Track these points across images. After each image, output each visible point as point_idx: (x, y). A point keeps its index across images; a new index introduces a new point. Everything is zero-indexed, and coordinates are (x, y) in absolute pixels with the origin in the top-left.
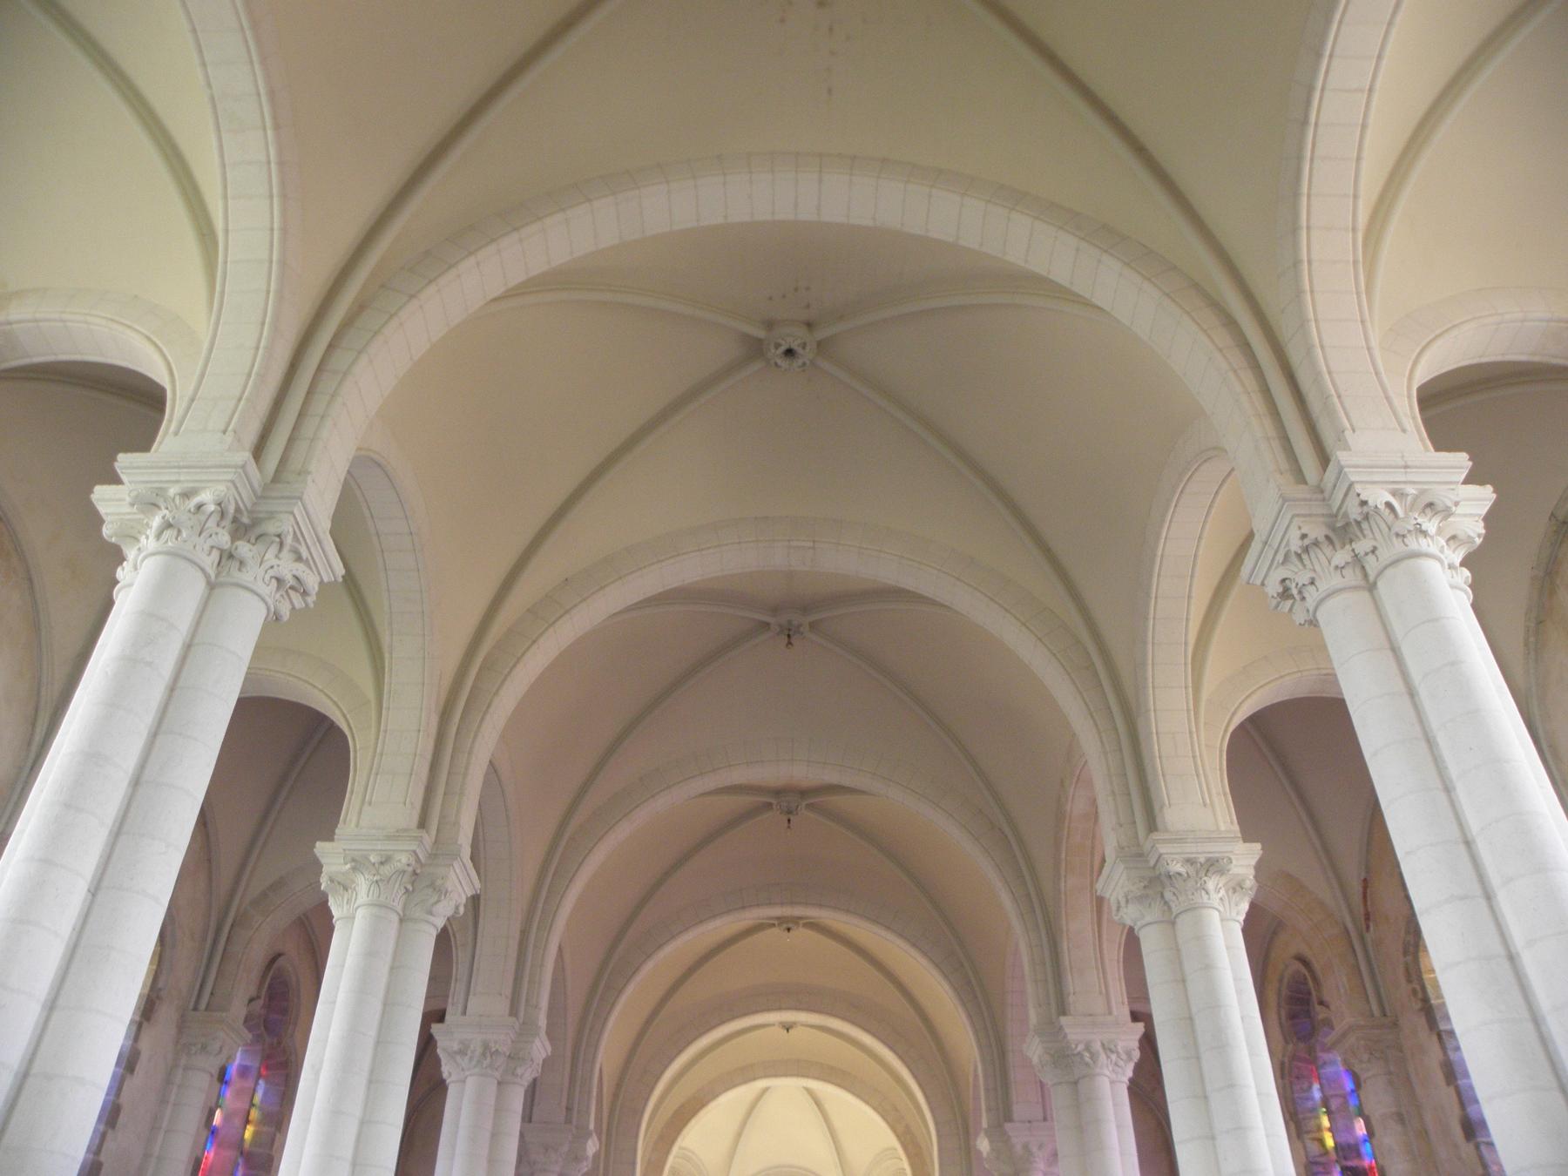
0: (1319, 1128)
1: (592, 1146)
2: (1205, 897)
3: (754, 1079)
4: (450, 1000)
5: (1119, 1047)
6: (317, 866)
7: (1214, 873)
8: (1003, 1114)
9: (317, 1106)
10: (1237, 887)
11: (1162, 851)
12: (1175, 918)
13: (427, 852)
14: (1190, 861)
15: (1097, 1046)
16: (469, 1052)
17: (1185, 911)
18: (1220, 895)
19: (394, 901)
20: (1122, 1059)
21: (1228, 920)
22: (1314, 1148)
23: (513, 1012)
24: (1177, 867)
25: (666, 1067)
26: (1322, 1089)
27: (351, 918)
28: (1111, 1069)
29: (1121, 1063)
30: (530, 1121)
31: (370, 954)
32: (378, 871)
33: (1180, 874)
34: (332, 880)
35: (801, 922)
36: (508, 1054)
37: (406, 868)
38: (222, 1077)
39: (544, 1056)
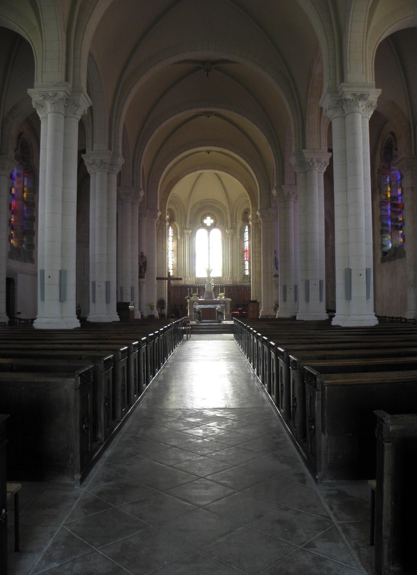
0: (387, 191)
1: (142, 193)
2: (357, 108)
3: (197, 170)
4: (87, 146)
5: (322, 161)
6: (30, 99)
7: (361, 100)
8: (282, 181)
9: (47, 184)
10: (370, 105)
11: (344, 90)
12: (345, 116)
13: (70, 91)
14: (354, 95)
15: (315, 160)
16: (96, 164)
17: (350, 113)
18: (363, 108)
19: (61, 110)
20: (323, 165)
21: (365, 117)
22: (384, 197)
23: (110, 148)
24: (349, 97)
25: (166, 167)
26: (390, 179)
27: (46, 118)
28: (318, 168)
29: (322, 166)
30: (120, 186)
31: (55, 131)
32: (53, 99)
33: (349, 99)
34: (36, 104)
35: (213, 113)
36: (110, 163)
37: (63, 97)
38: (12, 177)
39: (122, 164)
